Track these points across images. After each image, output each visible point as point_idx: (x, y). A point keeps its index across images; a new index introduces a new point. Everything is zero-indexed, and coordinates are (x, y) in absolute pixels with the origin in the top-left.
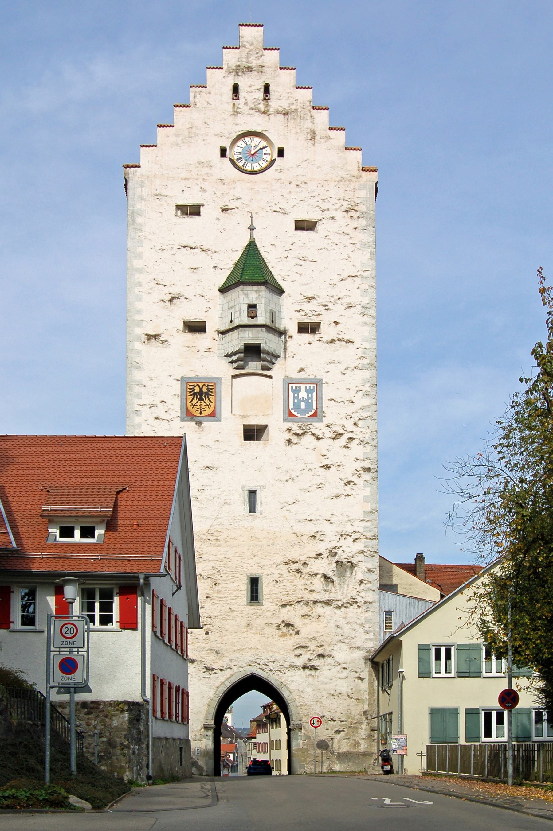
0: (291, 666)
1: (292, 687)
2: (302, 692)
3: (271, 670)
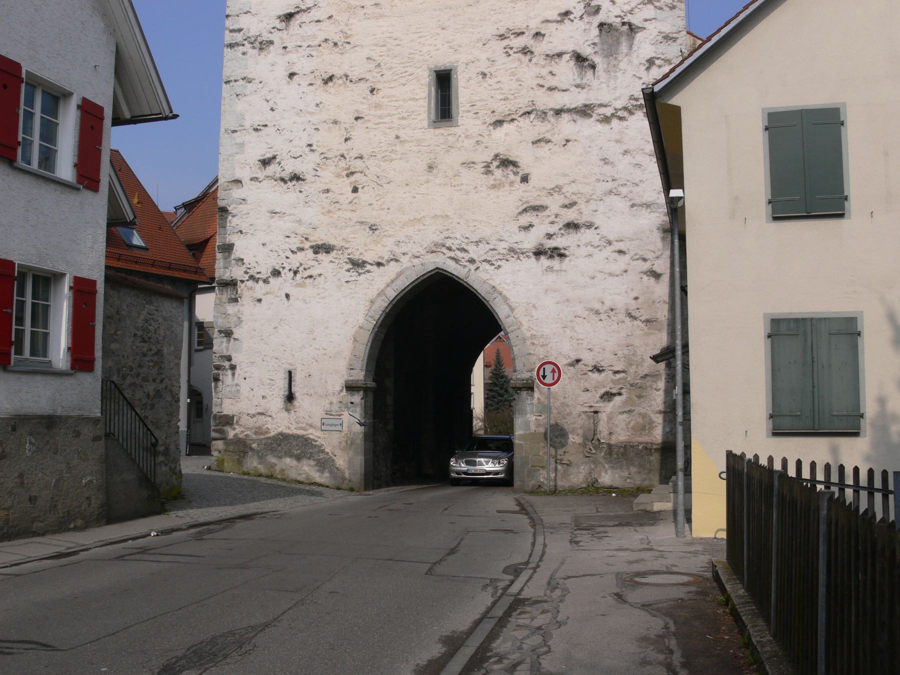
0: (512, 250)
3: (472, 261)
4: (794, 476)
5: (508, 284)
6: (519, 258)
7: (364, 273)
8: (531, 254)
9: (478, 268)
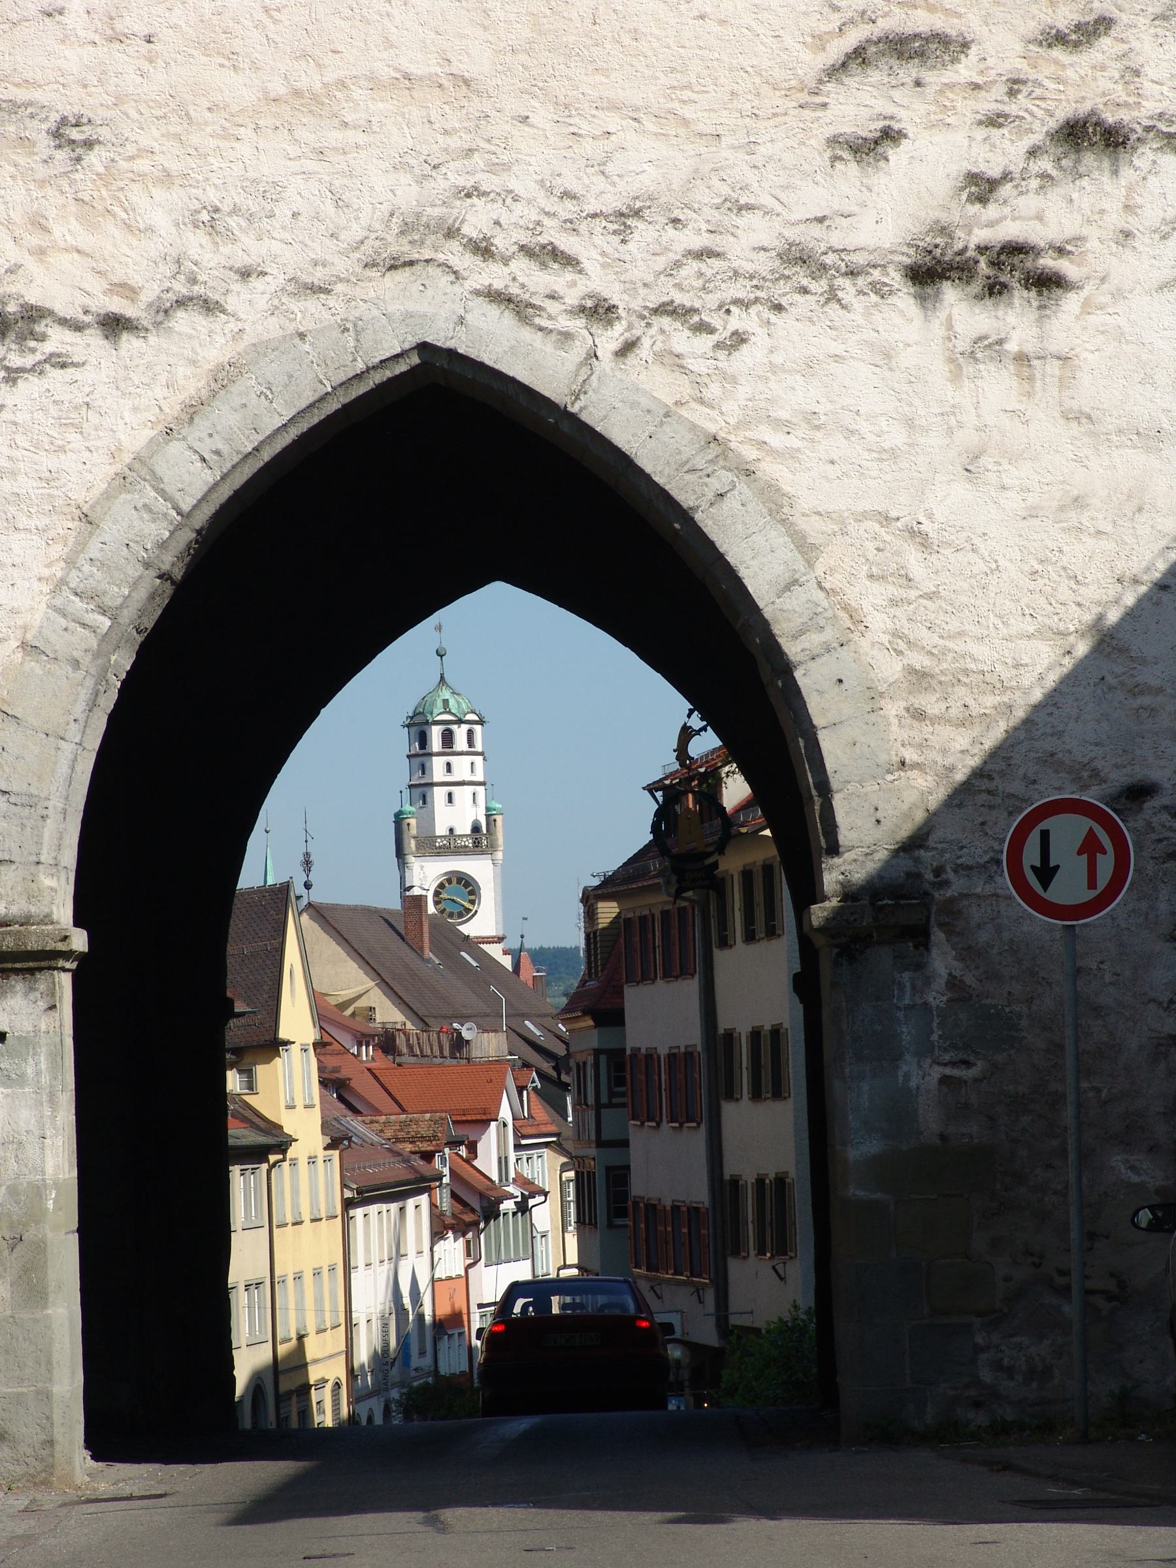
0: (798, 257)
1: (810, 486)
2: (915, 534)
3: (600, 311)
4: (274, 1426)
5: (786, 427)
6: (832, 296)
7: (37, 370)
8: (895, 278)
9: (627, 348)
